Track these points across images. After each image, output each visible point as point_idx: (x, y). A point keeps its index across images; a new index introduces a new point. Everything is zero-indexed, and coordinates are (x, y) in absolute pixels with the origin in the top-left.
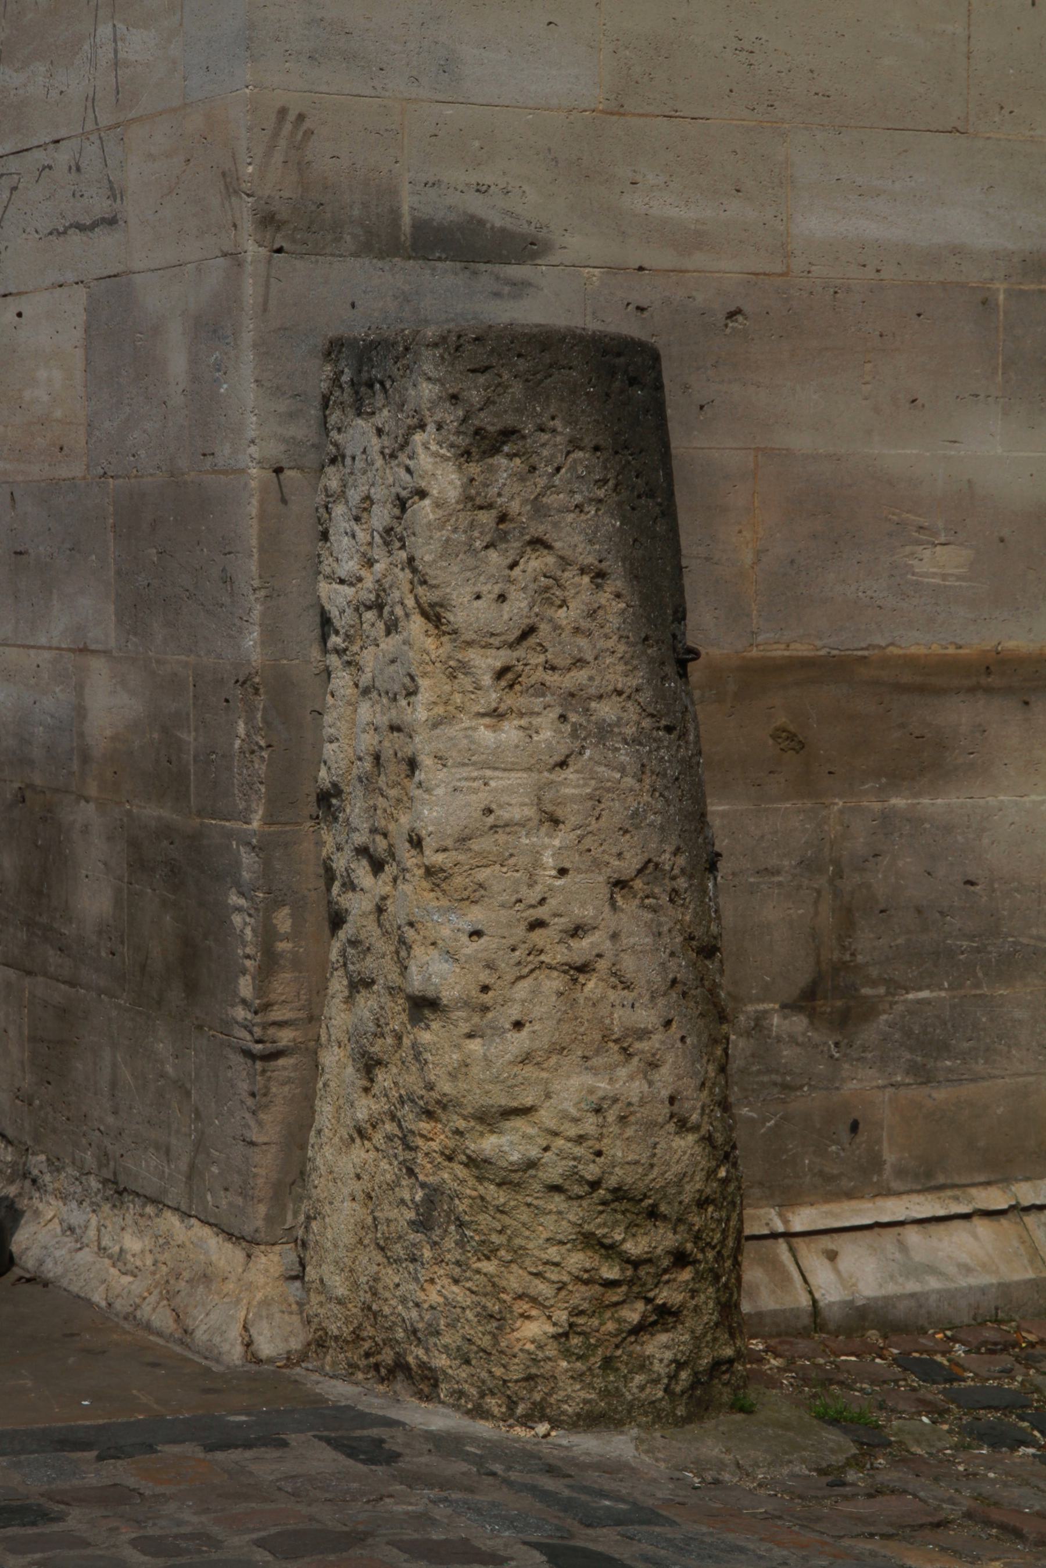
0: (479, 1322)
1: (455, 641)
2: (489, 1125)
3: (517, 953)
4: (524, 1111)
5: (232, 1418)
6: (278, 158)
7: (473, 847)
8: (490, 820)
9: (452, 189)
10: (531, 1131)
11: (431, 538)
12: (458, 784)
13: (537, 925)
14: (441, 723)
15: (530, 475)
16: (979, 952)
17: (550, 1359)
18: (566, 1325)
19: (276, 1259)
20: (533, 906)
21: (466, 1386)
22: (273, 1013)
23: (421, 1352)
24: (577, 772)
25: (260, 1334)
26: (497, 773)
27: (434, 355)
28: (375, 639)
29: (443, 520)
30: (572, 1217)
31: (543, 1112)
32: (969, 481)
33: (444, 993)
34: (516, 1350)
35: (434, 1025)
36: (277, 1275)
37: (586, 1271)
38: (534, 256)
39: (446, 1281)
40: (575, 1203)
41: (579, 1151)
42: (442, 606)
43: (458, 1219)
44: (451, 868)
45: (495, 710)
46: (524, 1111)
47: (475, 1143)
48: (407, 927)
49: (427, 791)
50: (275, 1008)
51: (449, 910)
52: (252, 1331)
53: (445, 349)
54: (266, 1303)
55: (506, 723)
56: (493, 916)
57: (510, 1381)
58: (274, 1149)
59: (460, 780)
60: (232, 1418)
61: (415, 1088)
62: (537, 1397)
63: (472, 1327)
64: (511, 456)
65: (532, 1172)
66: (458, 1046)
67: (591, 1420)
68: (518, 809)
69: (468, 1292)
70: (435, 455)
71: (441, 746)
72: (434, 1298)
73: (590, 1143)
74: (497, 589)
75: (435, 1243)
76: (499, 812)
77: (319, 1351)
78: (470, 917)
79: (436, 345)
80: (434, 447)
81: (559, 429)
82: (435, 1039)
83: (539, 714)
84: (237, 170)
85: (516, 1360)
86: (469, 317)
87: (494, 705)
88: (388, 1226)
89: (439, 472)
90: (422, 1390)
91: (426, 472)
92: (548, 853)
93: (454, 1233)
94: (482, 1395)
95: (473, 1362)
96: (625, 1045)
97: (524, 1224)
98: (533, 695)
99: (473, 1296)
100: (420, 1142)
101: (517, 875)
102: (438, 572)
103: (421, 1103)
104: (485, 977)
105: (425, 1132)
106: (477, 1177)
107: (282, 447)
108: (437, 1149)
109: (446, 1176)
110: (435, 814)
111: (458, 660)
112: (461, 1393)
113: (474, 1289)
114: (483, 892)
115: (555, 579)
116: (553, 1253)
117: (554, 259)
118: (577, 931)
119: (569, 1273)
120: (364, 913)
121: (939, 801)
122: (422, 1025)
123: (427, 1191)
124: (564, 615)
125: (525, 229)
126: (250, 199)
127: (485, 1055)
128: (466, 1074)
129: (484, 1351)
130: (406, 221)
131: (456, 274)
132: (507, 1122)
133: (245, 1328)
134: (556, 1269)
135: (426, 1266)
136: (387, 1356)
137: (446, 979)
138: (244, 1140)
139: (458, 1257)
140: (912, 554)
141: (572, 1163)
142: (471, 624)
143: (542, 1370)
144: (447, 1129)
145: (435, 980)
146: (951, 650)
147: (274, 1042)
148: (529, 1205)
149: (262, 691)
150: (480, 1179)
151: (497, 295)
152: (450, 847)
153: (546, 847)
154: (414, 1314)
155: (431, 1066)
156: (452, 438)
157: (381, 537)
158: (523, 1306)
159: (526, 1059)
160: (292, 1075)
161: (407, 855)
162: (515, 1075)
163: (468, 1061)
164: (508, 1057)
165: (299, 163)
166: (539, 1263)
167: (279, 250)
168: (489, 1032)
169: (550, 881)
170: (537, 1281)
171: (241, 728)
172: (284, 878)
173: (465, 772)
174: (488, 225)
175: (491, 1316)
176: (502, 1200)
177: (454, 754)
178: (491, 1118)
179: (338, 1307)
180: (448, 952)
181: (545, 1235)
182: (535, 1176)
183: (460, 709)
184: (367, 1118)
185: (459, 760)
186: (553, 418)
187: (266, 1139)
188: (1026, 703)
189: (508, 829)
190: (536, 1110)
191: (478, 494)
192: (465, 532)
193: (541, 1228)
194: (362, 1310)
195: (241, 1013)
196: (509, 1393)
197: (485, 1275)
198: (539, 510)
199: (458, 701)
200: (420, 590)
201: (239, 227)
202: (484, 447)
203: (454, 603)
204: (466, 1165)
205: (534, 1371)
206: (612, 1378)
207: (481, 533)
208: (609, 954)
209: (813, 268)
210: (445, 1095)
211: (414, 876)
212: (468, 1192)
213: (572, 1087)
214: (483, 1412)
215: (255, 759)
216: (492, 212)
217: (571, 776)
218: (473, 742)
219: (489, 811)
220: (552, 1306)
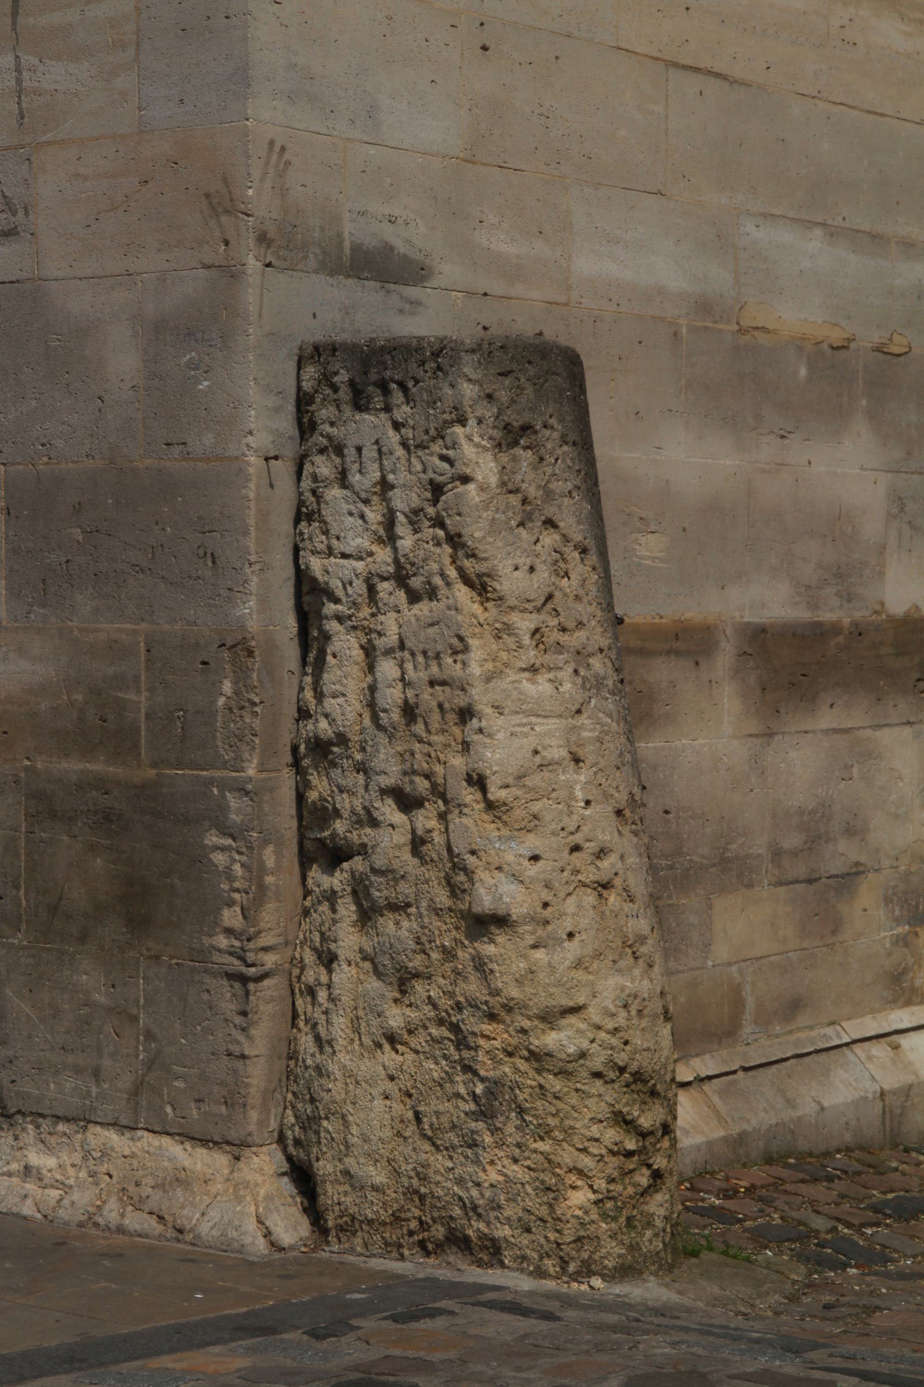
0: (537, 1194)
1: (500, 606)
2: (550, 1023)
3: (565, 874)
4: (576, 1010)
5: (348, 1296)
6: (268, 184)
7: (527, 783)
8: (538, 759)
9: (374, 219)
10: (583, 1026)
11: (480, 517)
12: (514, 729)
13: (576, 848)
14: (493, 678)
15: (539, 465)
16: (671, 869)
17: (593, 1222)
18: (605, 1191)
19: (267, 1158)
20: (572, 833)
21: (528, 1252)
22: (261, 939)
23: (482, 1226)
24: (589, 718)
25: (276, 1225)
26: (540, 720)
27: (473, 360)
28: (396, 606)
29: (487, 502)
30: (608, 1099)
31: (591, 1009)
32: (667, 481)
33: (513, 911)
34: (569, 1216)
35: (500, 939)
36: (271, 1173)
37: (616, 1144)
38: (424, 279)
39: (506, 1162)
40: (609, 1086)
41: (614, 1041)
42: (489, 576)
43: (519, 1107)
44: (512, 802)
45: (533, 666)
46: (576, 1010)
47: (538, 1039)
48: (468, 855)
49: (490, 736)
50: (262, 935)
51: (510, 838)
52: (267, 1224)
53: (482, 355)
54: (268, 1198)
55: (539, 677)
56: (547, 842)
57: (563, 1244)
58: (262, 1061)
59: (514, 726)
60: (348, 1296)
61: (478, 994)
62: (585, 1256)
63: (531, 1200)
64: (525, 448)
65: (582, 1062)
66: (525, 957)
67: (625, 1271)
68: (557, 752)
69: (526, 1170)
70: (478, 446)
71: (497, 697)
72: (493, 1176)
73: (622, 1034)
74: (528, 562)
75: (498, 1129)
76: (545, 753)
77: (341, 1235)
78: (527, 844)
79: (473, 351)
80: (477, 439)
81: (556, 426)
82: (502, 951)
83: (561, 668)
84: (230, 192)
85: (569, 1225)
86: (385, 329)
87: (532, 661)
88: (438, 1118)
89: (481, 461)
90: (481, 1258)
91: (470, 461)
92: (578, 787)
93: (514, 1119)
94: (541, 1258)
95: (534, 1230)
96: (635, 949)
97: (573, 1107)
98: (555, 653)
99: (531, 1173)
100: (481, 1042)
101: (560, 806)
102: (488, 546)
103: (485, 1008)
104: (546, 896)
105: (488, 1033)
106: (536, 1069)
107: (271, 439)
108: (499, 1047)
109: (507, 1070)
110: (498, 755)
111: (504, 623)
112: (524, 1258)
113: (533, 1166)
114: (537, 822)
115: (562, 555)
116: (595, 1130)
117: (434, 283)
118: (601, 853)
119: (606, 1146)
120: (396, 846)
121: (650, 744)
122: (486, 939)
123: (487, 1084)
124: (567, 585)
125: (419, 257)
126: (251, 219)
127: (550, 963)
128: (532, 980)
129: (542, 1220)
130: (347, 244)
131: (377, 292)
132: (564, 1020)
133: (260, 1222)
134: (596, 1144)
135: (488, 1150)
136: (439, 1232)
137: (515, 898)
138: (229, 1055)
139: (519, 1140)
140: (636, 540)
141: (610, 1052)
142: (514, 592)
143: (588, 1232)
144: (511, 1028)
145: (506, 899)
146: (657, 621)
147: (262, 965)
148: (577, 1090)
149: (257, 653)
150: (539, 1071)
151: (401, 311)
152: (511, 784)
153: (576, 782)
154: (475, 1193)
155: (498, 975)
156: (491, 431)
157: (406, 516)
158: (572, 1178)
159: (578, 964)
160: (274, 994)
161: (464, 792)
162: (572, 979)
163: (534, 968)
164: (567, 963)
165: (281, 189)
166: (585, 1140)
167: (269, 265)
168: (551, 942)
169: (582, 811)
170: (582, 1156)
171: (227, 687)
172: (270, 818)
173: (517, 719)
174: (396, 252)
175: (548, 1189)
176: (558, 1088)
177: (510, 703)
178: (550, 1018)
179: (374, 1194)
180: (514, 875)
181: (589, 1116)
182: (583, 1065)
183: (506, 665)
184: (403, 1025)
185: (513, 709)
186: (551, 417)
187: (256, 1052)
188: (697, 663)
189: (550, 768)
190: (586, 1008)
191: (510, 480)
192: (504, 512)
193: (586, 1110)
194: (404, 1194)
195: (222, 941)
196: (562, 1254)
197: (542, 1153)
198: (549, 495)
199: (505, 658)
200: (467, 564)
201: (232, 242)
202: (509, 440)
203: (500, 573)
204: (527, 1059)
205: (582, 1233)
206: (633, 1235)
207: (514, 513)
208: (621, 872)
209: (583, 300)
210: (512, 999)
211: (473, 810)
212: (529, 1082)
213: (610, 987)
214: (541, 1273)
215: (244, 714)
216: (399, 239)
217: (586, 722)
218: (521, 693)
219: (536, 752)
220: (594, 1176)
